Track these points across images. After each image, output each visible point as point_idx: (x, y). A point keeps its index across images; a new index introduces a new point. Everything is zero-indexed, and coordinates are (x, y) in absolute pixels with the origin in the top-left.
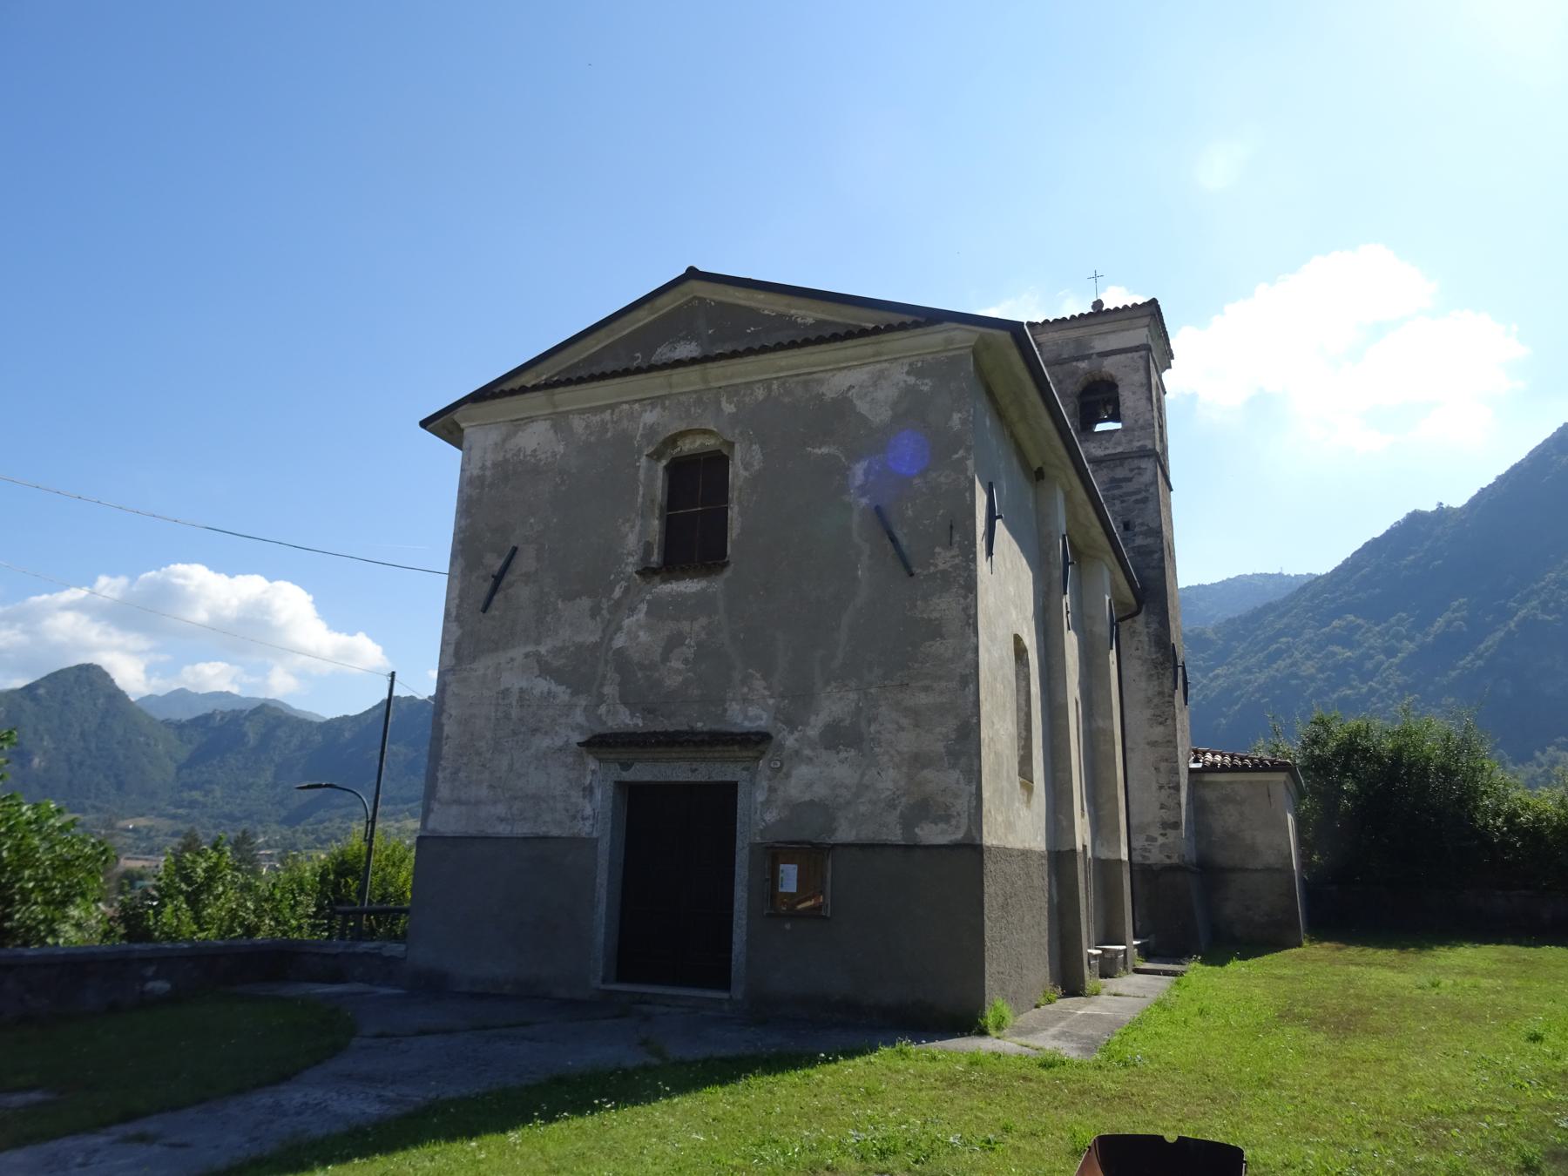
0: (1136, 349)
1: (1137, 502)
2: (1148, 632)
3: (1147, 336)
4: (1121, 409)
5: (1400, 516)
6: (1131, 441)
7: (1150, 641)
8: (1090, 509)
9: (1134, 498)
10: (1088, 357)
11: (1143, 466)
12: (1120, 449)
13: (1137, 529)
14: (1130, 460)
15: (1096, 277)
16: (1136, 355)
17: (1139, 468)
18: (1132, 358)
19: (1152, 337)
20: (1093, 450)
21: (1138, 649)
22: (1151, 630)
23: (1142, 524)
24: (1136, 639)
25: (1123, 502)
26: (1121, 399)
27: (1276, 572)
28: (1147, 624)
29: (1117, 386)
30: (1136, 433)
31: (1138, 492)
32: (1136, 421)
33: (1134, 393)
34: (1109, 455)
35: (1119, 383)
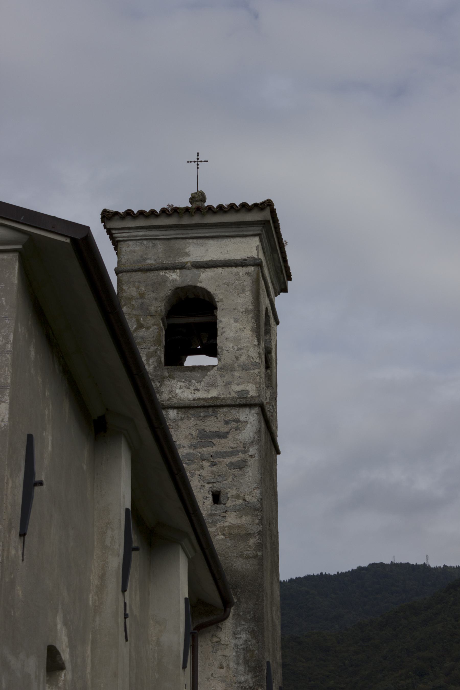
0: (242, 264)
1: (232, 465)
2: (236, 645)
3: (257, 247)
4: (219, 340)
5: (307, 575)
6: (228, 384)
7: (237, 656)
8: (165, 475)
9: (228, 460)
10: (182, 267)
11: (242, 418)
12: (213, 393)
13: (229, 503)
14: (225, 409)
15: (198, 161)
16: (241, 271)
17: (237, 421)
18: (237, 274)
19: (263, 249)
20: (178, 391)
21: (222, 668)
22: (241, 642)
23: (237, 497)
24: (219, 653)
25: (213, 464)
26: (220, 326)
27: (420, 562)
28: (235, 634)
29: (216, 308)
30: (237, 374)
31: (234, 452)
32: (237, 358)
33: (236, 321)
34: (199, 399)
35: (218, 305)
